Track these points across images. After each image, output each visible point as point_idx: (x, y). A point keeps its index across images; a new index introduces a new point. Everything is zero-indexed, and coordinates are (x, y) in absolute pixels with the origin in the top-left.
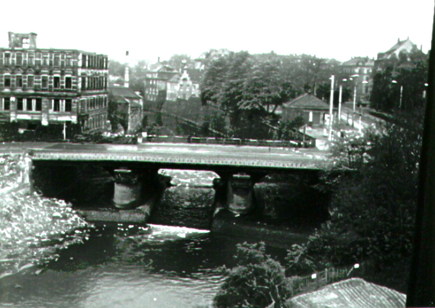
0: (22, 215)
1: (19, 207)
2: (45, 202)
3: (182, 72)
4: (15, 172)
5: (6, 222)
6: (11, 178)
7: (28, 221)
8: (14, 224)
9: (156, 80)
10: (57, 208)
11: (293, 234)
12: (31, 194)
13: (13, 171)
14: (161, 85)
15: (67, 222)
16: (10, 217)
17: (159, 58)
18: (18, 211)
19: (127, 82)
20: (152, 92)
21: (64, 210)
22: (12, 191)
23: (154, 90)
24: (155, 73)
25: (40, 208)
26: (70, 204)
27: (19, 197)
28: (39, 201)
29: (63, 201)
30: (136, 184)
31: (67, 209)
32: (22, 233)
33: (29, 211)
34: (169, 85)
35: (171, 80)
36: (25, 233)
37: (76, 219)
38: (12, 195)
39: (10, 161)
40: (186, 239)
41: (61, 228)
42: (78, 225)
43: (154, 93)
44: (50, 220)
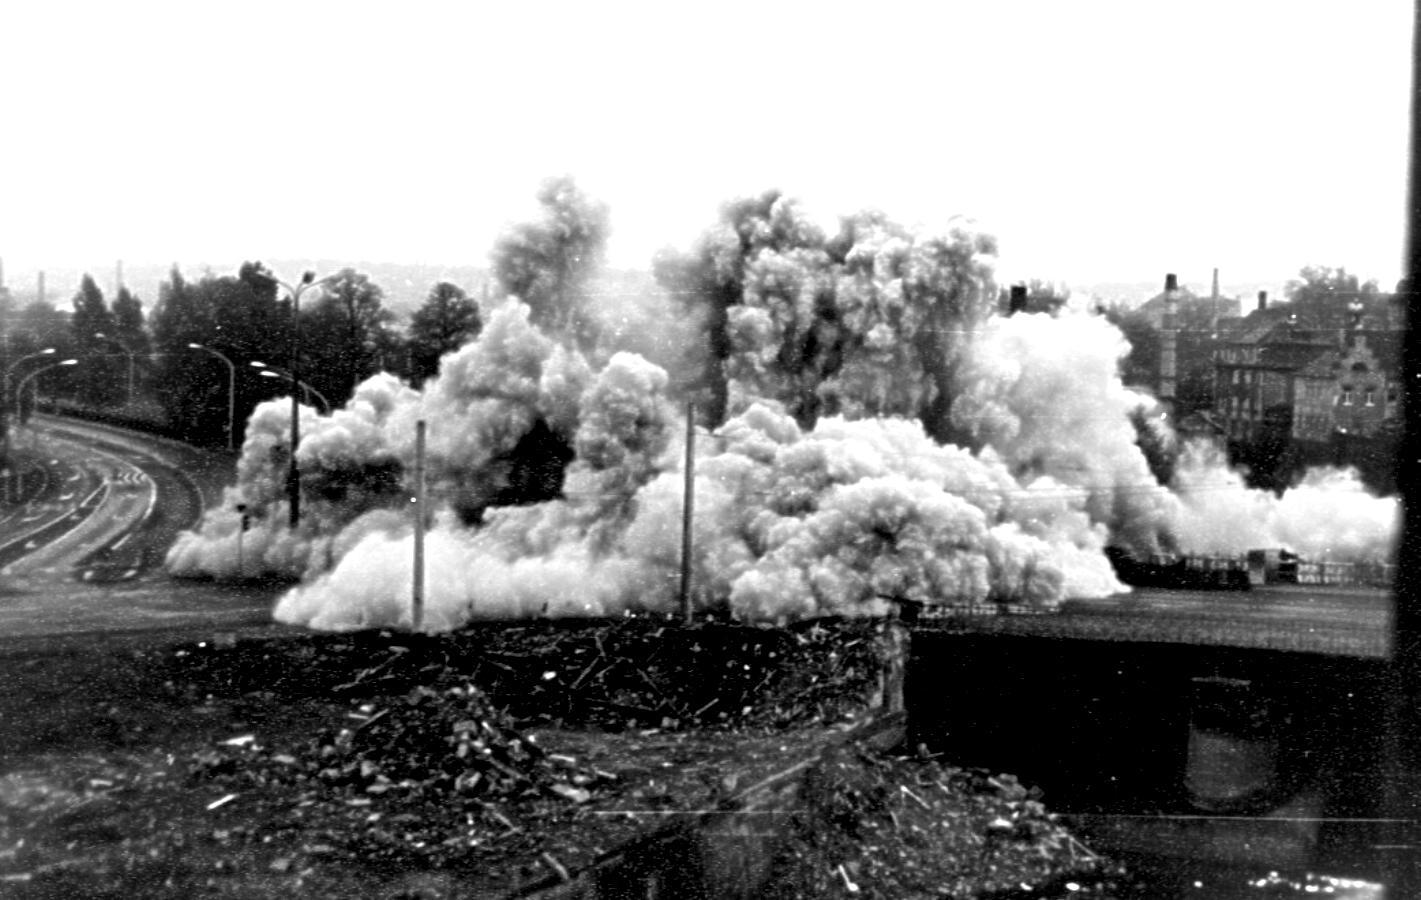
0: (890, 819)
1: (881, 792)
2: (955, 778)
3: (1351, 343)
5: (845, 840)
6: (854, 692)
7: (911, 840)
8: (867, 850)
9: (1255, 369)
10: (998, 802)
11: (213, 613)
12: (912, 750)
13: (856, 672)
14: (1271, 385)
15: (1037, 852)
16: (856, 824)
18: (877, 803)
19: (1168, 379)
20: (1240, 409)
21: (1019, 809)
22: (855, 736)
23: (1246, 404)
24: (1251, 346)
25: (942, 796)
26: (1035, 790)
27: (878, 757)
28: (937, 775)
30: (1264, 731)
31: (1030, 804)
32: (893, 882)
33: (909, 807)
34: (1300, 388)
35: (1309, 370)
36: (903, 882)
37: (1064, 842)
38: (856, 748)
39: (846, 637)
41: (1015, 870)
42: (1072, 863)
43: (1245, 416)
44: (979, 840)
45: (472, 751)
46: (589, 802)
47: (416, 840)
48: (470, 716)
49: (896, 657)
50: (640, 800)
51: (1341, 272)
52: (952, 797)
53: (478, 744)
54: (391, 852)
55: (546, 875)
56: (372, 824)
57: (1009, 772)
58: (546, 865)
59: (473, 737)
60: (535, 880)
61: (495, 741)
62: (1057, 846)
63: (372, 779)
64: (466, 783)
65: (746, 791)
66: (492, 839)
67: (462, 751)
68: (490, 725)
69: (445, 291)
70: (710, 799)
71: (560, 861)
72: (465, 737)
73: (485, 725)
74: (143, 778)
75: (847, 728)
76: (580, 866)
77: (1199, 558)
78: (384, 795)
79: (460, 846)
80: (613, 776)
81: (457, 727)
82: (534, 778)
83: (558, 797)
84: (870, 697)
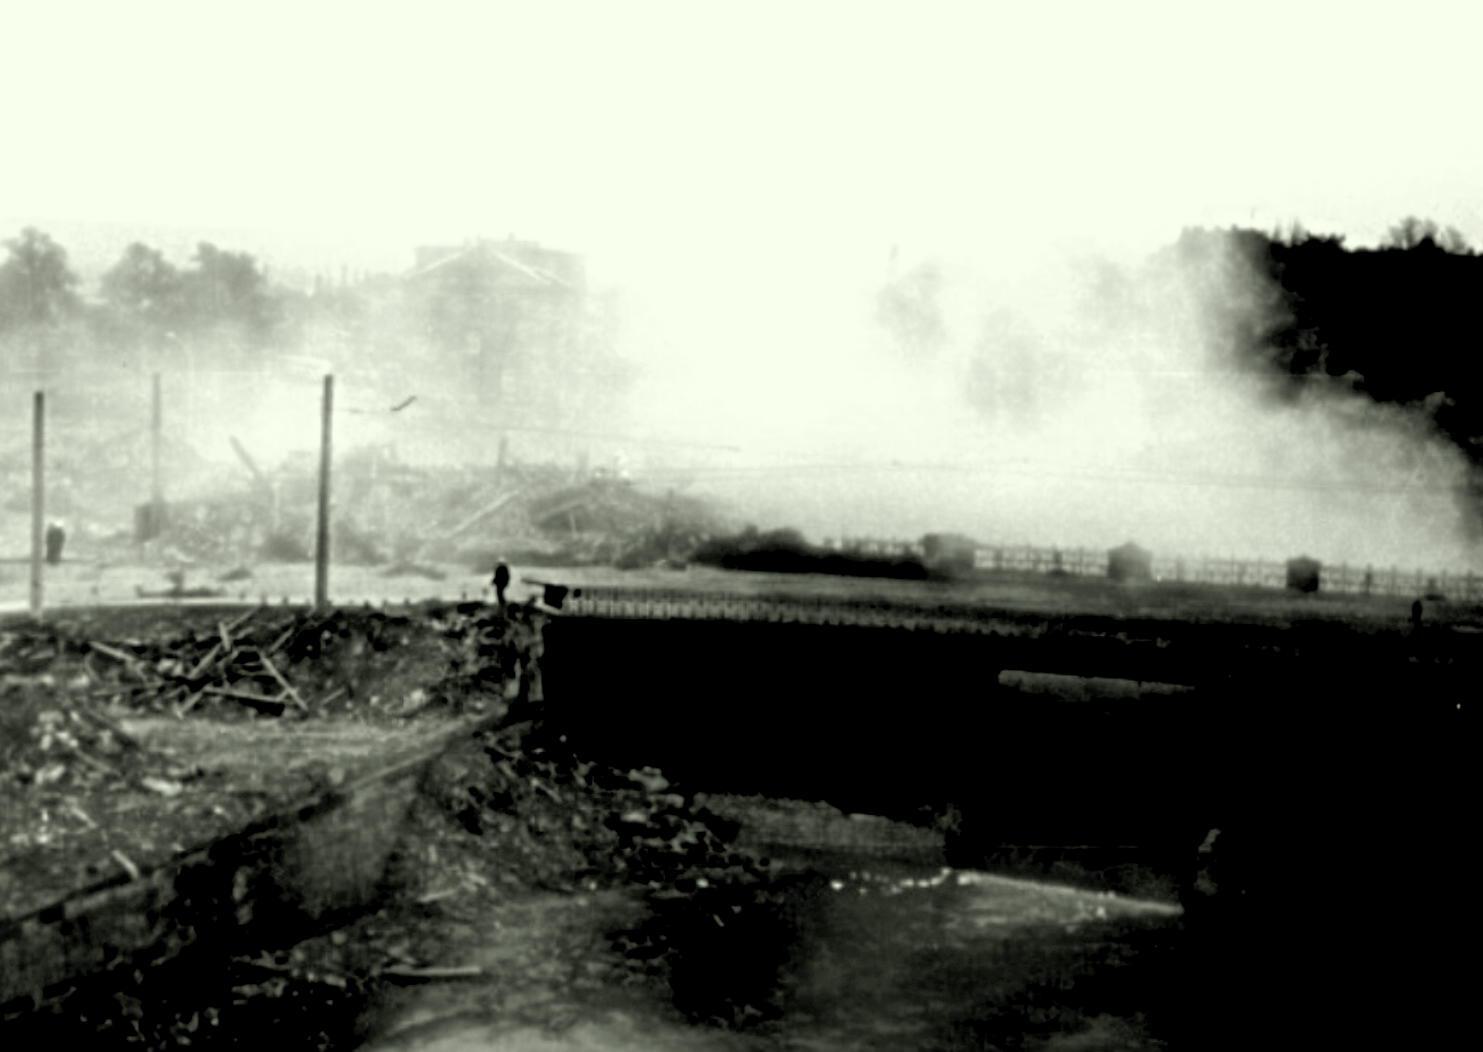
45: (57, 743)
46: (179, 796)
48: (57, 706)
49: (535, 645)
50: (233, 794)
52: (588, 791)
53: (64, 736)
55: (112, 874)
58: (115, 863)
67: (46, 743)
69: (138, 251)
70: (312, 792)
72: (49, 727)
75: (475, 718)
80: (1061, 864)
83: (146, 791)
84: (504, 687)
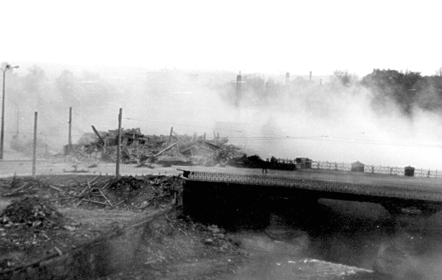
4: (169, 194)
15: (220, 249)
17: (311, 72)
26: (223, 230)
29: (216, 226)
37: (229, 246)
40: (310, 259)
45: (39, 215)
47: (17, 242)
51: (346, 73)
53: (41, 213)
54: (8, 245)
56: (3, 237)
57: (215, 224)
58: (55, 250)
59: (40, 210)
60: (50, 255)
61: (47, 212)
62: (226, 247)
63: (7, 223)
64: (36, 224)
65: (126, 229)
66: (40, 242)
67: (36, 215)
68: (46, 207)
71: (60, 249)
72: (37, 210)
73: (44, 207)
74: (238, 237)
76: (66, 251)
77: (282, 160)
78: (10, 228)
79: (29, 244)
81: (35, 207)
82: (58, 223)
83: (64, 229)
